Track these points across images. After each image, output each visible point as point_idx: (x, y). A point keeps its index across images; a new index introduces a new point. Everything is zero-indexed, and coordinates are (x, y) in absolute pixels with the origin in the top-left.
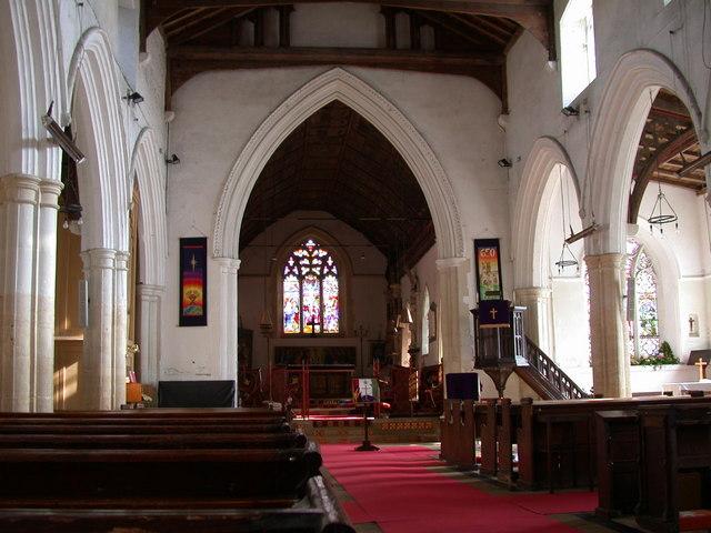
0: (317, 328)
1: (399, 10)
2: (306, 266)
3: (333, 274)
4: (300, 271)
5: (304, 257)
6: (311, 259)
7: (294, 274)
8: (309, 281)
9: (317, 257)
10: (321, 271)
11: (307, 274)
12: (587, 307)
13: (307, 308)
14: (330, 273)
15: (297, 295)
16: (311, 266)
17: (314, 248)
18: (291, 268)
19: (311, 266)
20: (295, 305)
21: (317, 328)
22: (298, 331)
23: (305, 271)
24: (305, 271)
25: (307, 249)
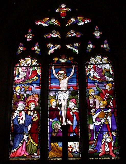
0: (75, 147)
1: (29, 115)
2: (55, 41)
3: (103, 53)
4: (44, 49)
5: (51, 28)
6: (63, 30)
7: (33, 55)
8: (59, 66)
9: (75, 27)
10: (82, 48)
11: (57, 53)
12: (96, 104)
13: (56, 113)
14: (98, 51)
15: (36, 89)
16: (64, 40)
17: (69, 16)
18: (29, 45)
19: (64, 40)
20: (32, 106)
21: (75, 147)
22: (36, 156)
23: (52, 49)
24: (52, 49)
25: (57, 16)
